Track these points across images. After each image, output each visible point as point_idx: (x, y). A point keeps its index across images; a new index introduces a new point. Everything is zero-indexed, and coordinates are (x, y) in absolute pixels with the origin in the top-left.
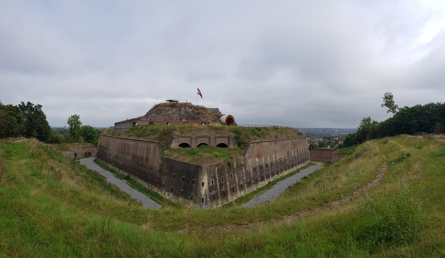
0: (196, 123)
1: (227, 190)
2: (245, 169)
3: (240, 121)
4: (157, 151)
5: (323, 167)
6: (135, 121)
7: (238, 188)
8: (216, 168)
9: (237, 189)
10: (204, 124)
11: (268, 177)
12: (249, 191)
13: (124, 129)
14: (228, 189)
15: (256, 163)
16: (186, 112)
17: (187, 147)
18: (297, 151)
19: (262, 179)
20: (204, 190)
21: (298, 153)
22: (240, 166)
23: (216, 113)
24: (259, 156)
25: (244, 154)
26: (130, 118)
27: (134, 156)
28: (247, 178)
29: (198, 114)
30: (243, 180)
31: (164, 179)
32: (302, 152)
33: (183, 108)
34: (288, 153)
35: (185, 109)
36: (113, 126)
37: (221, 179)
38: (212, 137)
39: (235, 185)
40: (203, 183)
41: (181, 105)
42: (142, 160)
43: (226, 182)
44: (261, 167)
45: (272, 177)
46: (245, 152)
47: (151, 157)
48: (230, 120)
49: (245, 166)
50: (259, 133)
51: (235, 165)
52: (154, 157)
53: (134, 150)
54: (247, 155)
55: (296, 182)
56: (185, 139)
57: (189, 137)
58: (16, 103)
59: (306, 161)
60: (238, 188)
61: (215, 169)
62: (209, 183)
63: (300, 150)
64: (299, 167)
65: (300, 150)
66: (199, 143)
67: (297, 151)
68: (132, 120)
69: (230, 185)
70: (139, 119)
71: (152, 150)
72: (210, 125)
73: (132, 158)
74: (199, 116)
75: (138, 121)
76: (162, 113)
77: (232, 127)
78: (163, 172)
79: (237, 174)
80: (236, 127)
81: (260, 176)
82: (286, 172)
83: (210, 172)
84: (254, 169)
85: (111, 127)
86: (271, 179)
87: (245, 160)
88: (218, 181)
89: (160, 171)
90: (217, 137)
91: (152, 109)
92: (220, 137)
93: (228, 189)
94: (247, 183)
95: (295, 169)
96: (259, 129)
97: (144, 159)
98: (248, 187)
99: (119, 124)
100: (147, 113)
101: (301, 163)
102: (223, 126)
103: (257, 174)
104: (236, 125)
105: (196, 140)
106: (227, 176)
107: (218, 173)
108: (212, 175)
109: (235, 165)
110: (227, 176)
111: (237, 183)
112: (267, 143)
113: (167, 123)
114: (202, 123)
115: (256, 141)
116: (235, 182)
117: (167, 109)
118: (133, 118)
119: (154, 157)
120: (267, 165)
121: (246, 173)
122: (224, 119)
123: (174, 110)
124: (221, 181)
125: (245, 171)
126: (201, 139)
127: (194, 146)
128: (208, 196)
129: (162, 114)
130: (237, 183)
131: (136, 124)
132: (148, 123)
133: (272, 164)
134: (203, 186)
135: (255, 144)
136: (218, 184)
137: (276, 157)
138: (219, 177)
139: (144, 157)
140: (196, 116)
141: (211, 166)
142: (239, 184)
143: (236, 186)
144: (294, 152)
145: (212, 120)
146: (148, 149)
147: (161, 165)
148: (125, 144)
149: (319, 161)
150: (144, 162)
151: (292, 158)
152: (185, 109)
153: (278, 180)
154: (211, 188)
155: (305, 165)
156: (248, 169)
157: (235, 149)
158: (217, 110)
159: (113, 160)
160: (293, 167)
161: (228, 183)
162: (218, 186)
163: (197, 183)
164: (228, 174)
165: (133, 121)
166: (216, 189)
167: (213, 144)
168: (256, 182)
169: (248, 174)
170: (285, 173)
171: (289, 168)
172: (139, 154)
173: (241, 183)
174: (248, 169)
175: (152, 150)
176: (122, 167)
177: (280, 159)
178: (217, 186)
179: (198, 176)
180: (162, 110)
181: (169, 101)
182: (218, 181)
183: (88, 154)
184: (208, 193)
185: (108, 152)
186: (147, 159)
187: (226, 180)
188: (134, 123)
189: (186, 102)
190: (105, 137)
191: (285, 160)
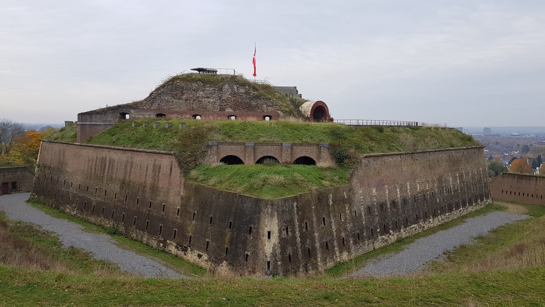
0: (253, 116)
1: (314, 248)
2: (350, 209)
3: (341, 114)
4: (177, 171)
5: (524, 217)
6: (125, 110)
7: (335, 243)
8: (295, 204)
9: (334, 247)
10: (267, 119)
11: (397, 228)
12: (357, 250)
13: (99, 128)
14: (318, 245)
15: (372, 197)
16: (234, 94)
17: (237, 163)
18: (461, 176)
19: (385, 230)
20: (269, 247)
21: (462, 181)
22: (341, 201)
23: (290, 99)
24: (380, 186)
25: (350, 180)
26: (112, 104)
27: (124, 184)
28: (354, 226)
29: (258, 97)
30: (345, 229)
31: (191, 226)
32: (473, 179)
33: (226, 86)
34: (440, 180)
35: (232, 88)
36: (75, 119)
37: (304, 225)
38: (285, 144)
39: (330, 238)
40: (269, 233)
41: (222, 79)
42: (144, 191)
43: (314, 232)
44: (382, 206)
45: (405, 227)
46: (352, 175)
47: (162, 184)
48: (320, 111)
49: (350, 201)
50: (379, 137)
51: (331, 200)
52: (170, 184)
53: (126, 172)
54: (355, 181)
55: (458, 244)
56: (233, 147)
57: (240, 144)
58: (135, 87)
59: (482, 200)
60: (335, 243)
61: (292, 206)
62: (280, 232)
63: (467, 174)
64: (462, 211)
65: (467, 174)
66: (259, 156)
67: (461, 176)
68: (119, 107)
69: (321, 238)
70: (135, 106)
71: (165, 169)
72: (282, 120)
73: (122, 188)
74: (259, 102)
75: (132, 111)
76: (183, 94)
77: (323, 124)
78: (190, 213)
79: (335, 216)
80: (331, 123)
81: (381, 224)
82: (436, 220)
83: (283, 211)
84: (369, 210)
85: (69, 124)
86: (404, 233)
87: (350, 190)
88: (297, 230)
89: (183, 211)
90: (295, 145)
91: (163, 86)
92: (301, 145)
93: (318, 245)
94: (353, 236)
95: (456, 214)
96: (380, 129)
97: (148, 189)
98: (355, 243)
99: (88, 117)
100: (151, 94)
101: (471, 204)
102: (308, 123)
103: (373, 219)
104: (332, 120)
105: (254, 149)
106: (315, 219)
107: (298, 214)
108: (287, 217)
109: (331, 200)
110: (315, 219)
111: (335, 234)
112: (395, 158)
113: (195, 116)
114: (264, 117)
115: (373, 154)
116: (331, 232)
117: (195, 85)
118: (120, 103)
119: (170, 184)
120: (394, 203)
121: (352, 216)
122: (307, 108)
123: (209, 89)
124: (304, 230)
125: (351, 212)
126: (265, 148)
127: (249, 163)
128: (279, 256)
129: (184, 97)
130: (335, 234)
131: (127, 116)
132: (153, 116)
133: (405, 201)
134: (269, 237)
135: (371, 160)
136: (298, 234)
137: (413, 188)
138: (301, 221)
139: (148, 186)
140: (254, 103)
141: (285, 200)
142: (339, 236)
143: (332, 240)
144: (455, 178)
145: (284, 112)
146: (157, 169)
147: (186, 200)
148: (103, 160)
149: (513, 202)
150: (148, 195)
151: (449, 191)
152: (232, 88)
153: (418, 236)
154: (283, 243)
155: (478, 207)
156: (355, 208)
157: (329, 169)
158: (294, 90)
159: (75, 196)
160: (450, 210)
161: (316, 235)
162: (299, 240)
163: (258, 233)
164: (317, 216)
165: (121, 111)
166: (294, 244)
167: (285, 157)
168: (373, 235)
169: (356, 218)
170: (434, 222)
171: (443, 212)
172: (136, 177)
173: (343, 235)
174: (355, 208)
175: (165, 169)
176: (100, 210)
177: (423, 191)
178: (296, 238)
179: (259, 219)
180: (183, 88)
181: (199, 70)
182: (297, 230)
183: (10, 186)
184: (278, 251)
185: (62, 179)
186: (154, 189)
187: (312, 227)
188: (123, 115)
189: (232, 74)
190: (52, 145)
191: (433, 195)
